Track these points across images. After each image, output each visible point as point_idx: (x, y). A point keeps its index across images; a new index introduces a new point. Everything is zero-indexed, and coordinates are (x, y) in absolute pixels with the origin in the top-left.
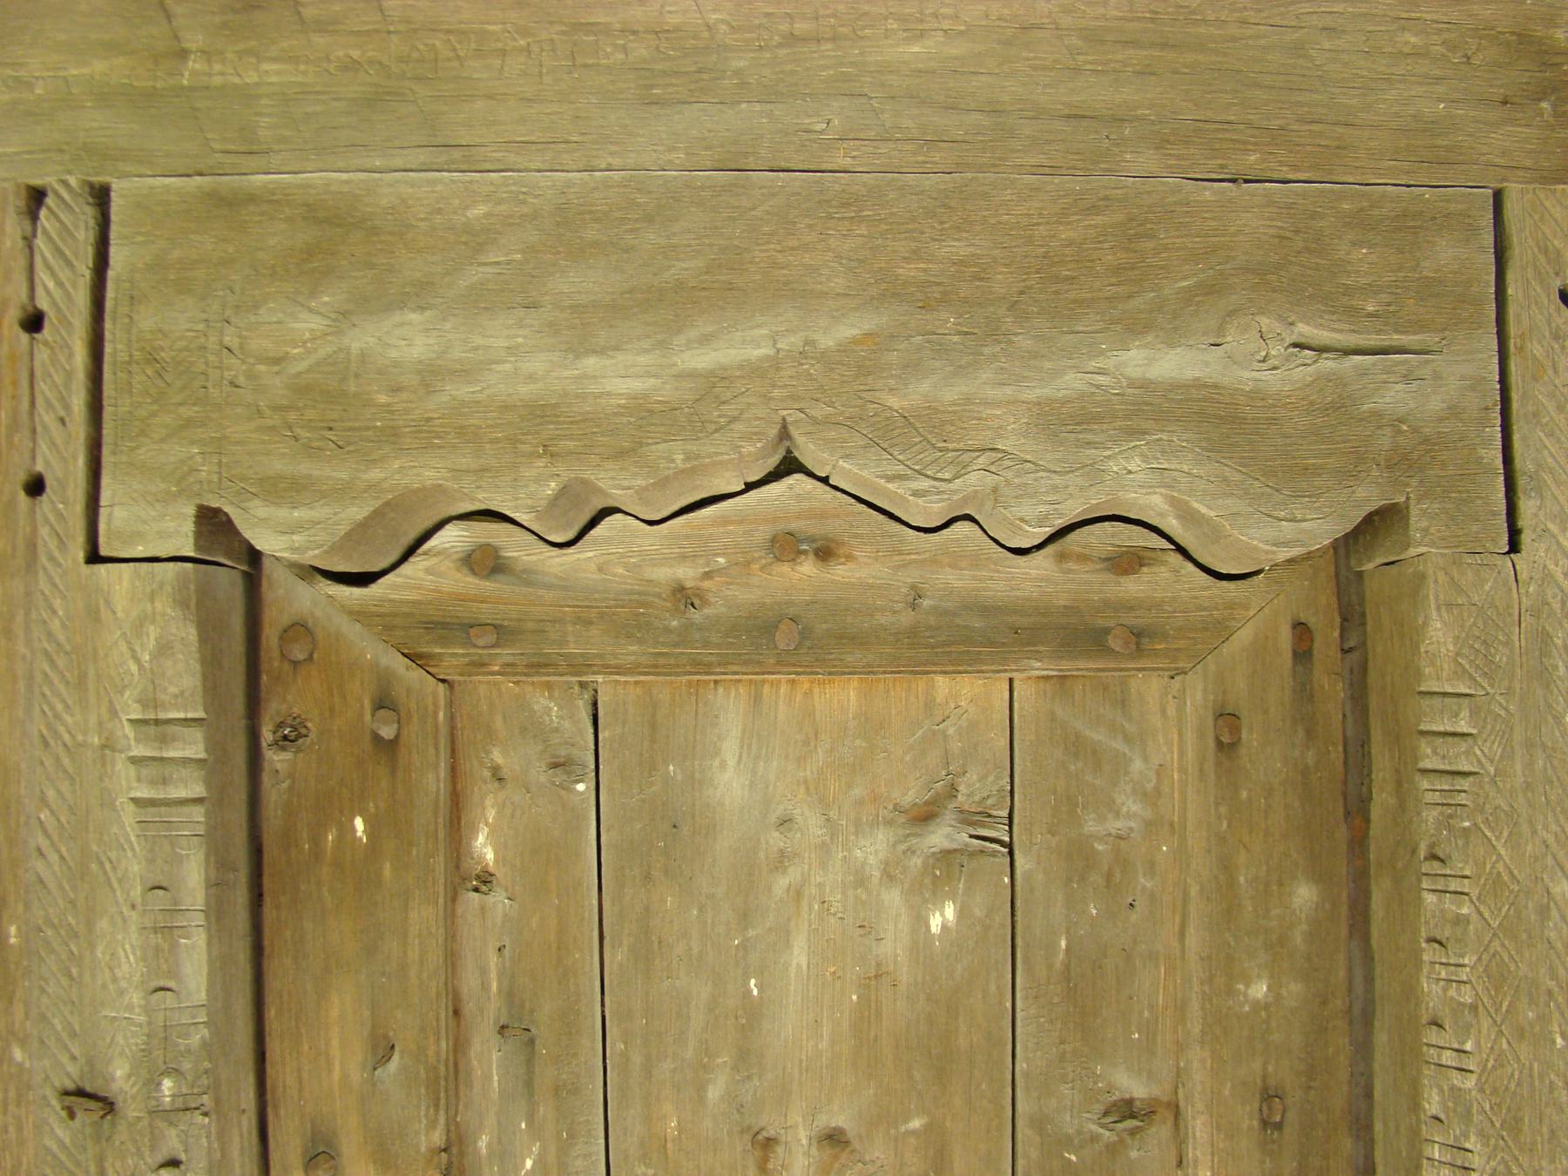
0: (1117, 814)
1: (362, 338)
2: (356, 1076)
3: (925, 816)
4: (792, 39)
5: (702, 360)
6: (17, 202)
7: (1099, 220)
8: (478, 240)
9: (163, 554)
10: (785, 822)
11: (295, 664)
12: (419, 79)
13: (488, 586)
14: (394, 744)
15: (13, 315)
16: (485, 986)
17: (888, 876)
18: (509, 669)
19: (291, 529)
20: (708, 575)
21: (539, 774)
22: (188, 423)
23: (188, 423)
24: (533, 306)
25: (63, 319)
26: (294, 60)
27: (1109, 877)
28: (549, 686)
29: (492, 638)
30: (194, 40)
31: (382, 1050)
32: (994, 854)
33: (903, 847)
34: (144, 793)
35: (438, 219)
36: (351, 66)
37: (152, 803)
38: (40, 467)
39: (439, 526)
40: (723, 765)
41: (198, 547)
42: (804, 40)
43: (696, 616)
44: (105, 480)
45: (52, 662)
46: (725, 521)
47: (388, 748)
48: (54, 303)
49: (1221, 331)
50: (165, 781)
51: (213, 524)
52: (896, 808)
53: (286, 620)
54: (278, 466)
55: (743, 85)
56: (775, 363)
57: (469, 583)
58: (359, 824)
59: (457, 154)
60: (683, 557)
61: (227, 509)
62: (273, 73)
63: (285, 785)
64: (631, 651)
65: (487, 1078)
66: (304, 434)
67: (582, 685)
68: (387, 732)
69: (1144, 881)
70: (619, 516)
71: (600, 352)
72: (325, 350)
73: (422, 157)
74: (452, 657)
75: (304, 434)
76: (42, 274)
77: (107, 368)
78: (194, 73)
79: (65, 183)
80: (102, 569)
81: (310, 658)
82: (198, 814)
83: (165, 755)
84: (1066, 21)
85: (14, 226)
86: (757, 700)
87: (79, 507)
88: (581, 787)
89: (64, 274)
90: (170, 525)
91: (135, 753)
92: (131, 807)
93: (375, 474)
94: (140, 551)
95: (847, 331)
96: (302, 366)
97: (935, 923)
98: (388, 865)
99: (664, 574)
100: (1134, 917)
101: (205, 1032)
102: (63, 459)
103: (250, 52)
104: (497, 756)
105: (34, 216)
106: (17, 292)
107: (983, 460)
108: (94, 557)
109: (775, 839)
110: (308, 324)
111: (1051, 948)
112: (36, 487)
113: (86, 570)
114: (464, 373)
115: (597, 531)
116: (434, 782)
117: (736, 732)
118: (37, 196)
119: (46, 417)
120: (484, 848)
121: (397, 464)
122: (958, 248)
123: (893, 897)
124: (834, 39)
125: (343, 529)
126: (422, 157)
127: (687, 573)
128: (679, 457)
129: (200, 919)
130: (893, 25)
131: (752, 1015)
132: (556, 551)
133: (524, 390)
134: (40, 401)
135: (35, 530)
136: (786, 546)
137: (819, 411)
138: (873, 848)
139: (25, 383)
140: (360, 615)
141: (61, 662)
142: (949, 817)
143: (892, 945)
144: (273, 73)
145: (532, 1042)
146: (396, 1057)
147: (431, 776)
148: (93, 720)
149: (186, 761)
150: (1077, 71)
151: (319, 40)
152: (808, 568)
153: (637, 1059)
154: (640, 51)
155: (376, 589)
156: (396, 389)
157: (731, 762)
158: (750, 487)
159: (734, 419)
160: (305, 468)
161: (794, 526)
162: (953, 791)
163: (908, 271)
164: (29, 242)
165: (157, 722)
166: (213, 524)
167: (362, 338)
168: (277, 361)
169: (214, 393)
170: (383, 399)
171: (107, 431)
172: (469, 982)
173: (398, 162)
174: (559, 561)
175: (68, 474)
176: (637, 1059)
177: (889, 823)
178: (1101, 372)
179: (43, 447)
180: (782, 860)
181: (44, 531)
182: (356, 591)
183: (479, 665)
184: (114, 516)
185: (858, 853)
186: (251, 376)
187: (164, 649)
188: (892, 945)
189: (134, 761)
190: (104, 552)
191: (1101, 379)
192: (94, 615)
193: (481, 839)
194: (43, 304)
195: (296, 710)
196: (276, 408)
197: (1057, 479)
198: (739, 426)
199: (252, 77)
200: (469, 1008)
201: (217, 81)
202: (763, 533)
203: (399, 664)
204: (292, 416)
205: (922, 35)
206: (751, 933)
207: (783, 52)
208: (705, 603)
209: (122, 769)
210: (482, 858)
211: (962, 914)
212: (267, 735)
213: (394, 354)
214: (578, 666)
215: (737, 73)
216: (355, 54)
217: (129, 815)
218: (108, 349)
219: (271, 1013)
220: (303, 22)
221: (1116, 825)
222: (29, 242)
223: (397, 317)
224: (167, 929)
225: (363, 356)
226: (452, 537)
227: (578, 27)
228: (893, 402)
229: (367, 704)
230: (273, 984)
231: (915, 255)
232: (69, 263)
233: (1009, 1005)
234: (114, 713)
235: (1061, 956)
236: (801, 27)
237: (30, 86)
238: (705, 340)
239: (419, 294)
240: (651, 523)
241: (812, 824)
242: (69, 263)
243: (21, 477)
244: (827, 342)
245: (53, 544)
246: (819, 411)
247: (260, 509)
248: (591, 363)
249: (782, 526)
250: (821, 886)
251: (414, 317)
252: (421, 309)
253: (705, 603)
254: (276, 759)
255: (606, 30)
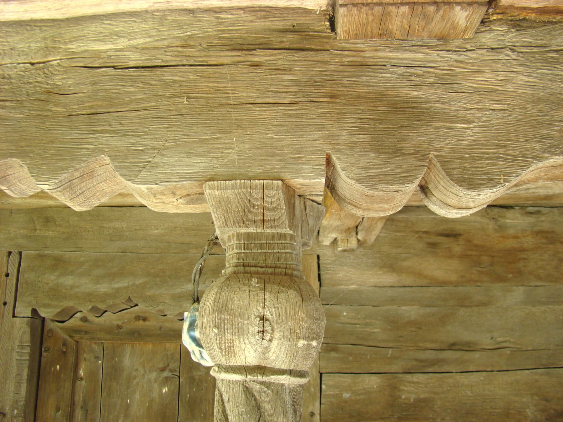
0: (200, 371)
1: (62, 280)
2: (53, 414)
3: (163, 370)
4: (136, 230)
5: (116, 286)
6: (6, 254)
7: (185, 262)
8: (82, 264)
9: (25, 316)
10: (137, 370)
11: (49, 337)
12: (74, 235)
13: (84, 324)
14: (66, 352)
15: (4, 274)
16: (79, 399)
17: (155, 381)
18: (87, 339)
19: (47, 313)
20: (123, 323)
21: (93, 359)
22: (32, 294)
23: (32, 294)
24: (90, 276)
25: (12, 275)
26: (54, 231)
27: (198, 384)
28: (96, 343)
29: (84, 333)
30: (38, 227)
31: (58, 409)
32: (176, 378)
33: (158, 376)
34: (18, 358)
35: (75, 260)
36: (63, 233)
37: (19, 360)
38: (6, 300)
39: (77, 313)
40: (126, 359)
41: (31, 315)
42: (138, 230)
43: (121, 330)
44: (17, 303)
45: (5, 335)
46: (127, 313)
47: (64, 353)
48: (11, 273)
49: (205, 281)
50: (22, 356)
51: (34, 311)
52: (158, 368)
53: (48, 329)
54: (46, 302)
55: (127, 238)
56: (128, 287)
57: (81, 323)
58: (58, 366)
59: (79, 249)
60: (119, 320)
61: (37, 309)
62: (50, 234)
63: (46, 359)
64: (109, 337)
65: (78, 417)
66: (51, 297)
67: (102, 343)
68: (64, 350)
69: (205, 385)
70: (108, 312)
71: (100, 284)
72: (55, 282)
73: (74, 249)
74: (77, 337)
75: (51, 297)
76: (9, 267)
77: (19, 284)
78: (38, 233)
79: (15, 251)
80: (15, 318)
81: (52, 336)
82: (27, 362)
83: (23, 351)
84: (182, 226)
85: (5, 259)
86: (133, 347)
87: (12, 307)
88: (100, 362)
89: (13, 267)
90: (27, 311)
91: (17, 351)
92: (15, 360)
93: (62, 304)
94: (22, 316)
95: (141, 281)
96: (51, 285)
97: (164, 391)
98: (62, 375)
99: (115, 323)
100: (203, 391)
101: (24, 402)
102: (10, 299)
103: (47, 230)
104: (85, 356)
105: (9, 257)
106: (4, 270)
107: (162, 304)
108: (14, 316)
109: (134, 373)
110: (53, 278)
111: (186, 397)
112: (5, 304)
113: (12, 318)
114: (78, 287)
115: (104, 315)
116: (72, 359)
117: (129, 353)
118: (10, 253)
119: (8, 292)
120: (82, 373)
121: (65, 302)
122: (160, 267)
123: (156, 385)
124: (143, 230)
125: (55, 313)
126: (74, 249)
127: (120, 323)
128: (111, 303)
129: (26, 381)
130: (153, 227)
131: (128, 406)
132: (96, 318)
133: (87, 290)
134: (7, 289)
135: (4, 312)
136: (138, 318)
137: (135, 295)
138: (153, 376)
139: (5, 286)
140: (61, 328)
141: (6, 334)
142: (167, 370)
143: (155, 395)
144: (50, 234)
145: (87, 410)
146: (60, 411)
147: (72, 359)
148: (10, 345)
149: (26, 353)
150: (183, 235)
151: (58, 228)
152: (141, 322)
153: (106, 414)
154: (111, 232)
155: (65, 324)
156: (66, 289)
157: (128, 358)
158: (132, 307)
159: (121, 296)
160: (50, 302)
161: (139, 314)
162: (168, 365)
163: (152, 271)
164: (8, 261)
165: (22, 346)
166: (34, 311)
167: (62, 280)
168: (47, 284)
169: (36, 289)
170: (64, 291)
171: (18, 294)
172: (77, 398)
173: (70, 250)
174: (97, 320)
175: (10, 302)
176: (106, 414)
177: (156, 371)
178: (183, 289)
179: (7, 297)
180: (135, 378)
181: (6, 312)
182: (61, 324)
183: (82, 338)
184: (18, 309)
185: (150, 377)
186: (43, 286)
187: (24, 333)
188: (155, 395)
189: (17, 352)
190: (16, 315)
191: (183, 290)
192: (13, 326)
193: (81, 371)
194: (9, 272)
195: (49, 345)
196: (48, 292)
197: (174, 308)
198: (122, 297)
199: (47, 234)
200: (76, 403)
201: (41, 234)
202: (133, 316)
203: (67, 337)
204: (49, 293)
205: (157, 229)
206: (129, 391)
207: (134, 232)
208: (122, 328)
209: (15, 354)
210: (81, 374)
211: (169, 389)
212: (43, 349)
213: (66, 283)
214: (99, 339)
215: (126, 236)
216: (64, 231)
217: (15, 362)
218: (19, 280)
219: (38, 402)
220: (56, 224)
221: (200, 373)
222: (8, 261)
223: (67, 277)
224: (19, 383)
225: (61, 284)
226: (78, 315)
227: (101, 227)
228: (148, 294)
229: (61, 345)
230: (39, 396)
231: (153, 268)
232: (14, 265)
233: (177, 408)
234: (14, 343)
235: (188, 398)
236: (138, 228)
237: (11, 234)
238: (117, 282)
239: (72, 273)
240: (114, 313)
241: (142, 371)
242: (14, 265)
243: (3, 302)
244: (137, 283)
245: (7, 314)
246: (135, 295)
247: (42, 309)
248: (99, 286)
249: (137, 314)
250: (142, 383)
251: (70, 277)
252: (71, 276)
253: (122, 328)
254: (44, 354)
255: (105, 228)
